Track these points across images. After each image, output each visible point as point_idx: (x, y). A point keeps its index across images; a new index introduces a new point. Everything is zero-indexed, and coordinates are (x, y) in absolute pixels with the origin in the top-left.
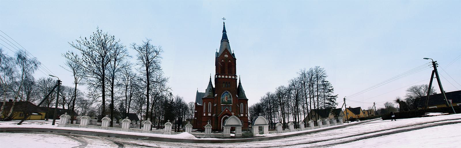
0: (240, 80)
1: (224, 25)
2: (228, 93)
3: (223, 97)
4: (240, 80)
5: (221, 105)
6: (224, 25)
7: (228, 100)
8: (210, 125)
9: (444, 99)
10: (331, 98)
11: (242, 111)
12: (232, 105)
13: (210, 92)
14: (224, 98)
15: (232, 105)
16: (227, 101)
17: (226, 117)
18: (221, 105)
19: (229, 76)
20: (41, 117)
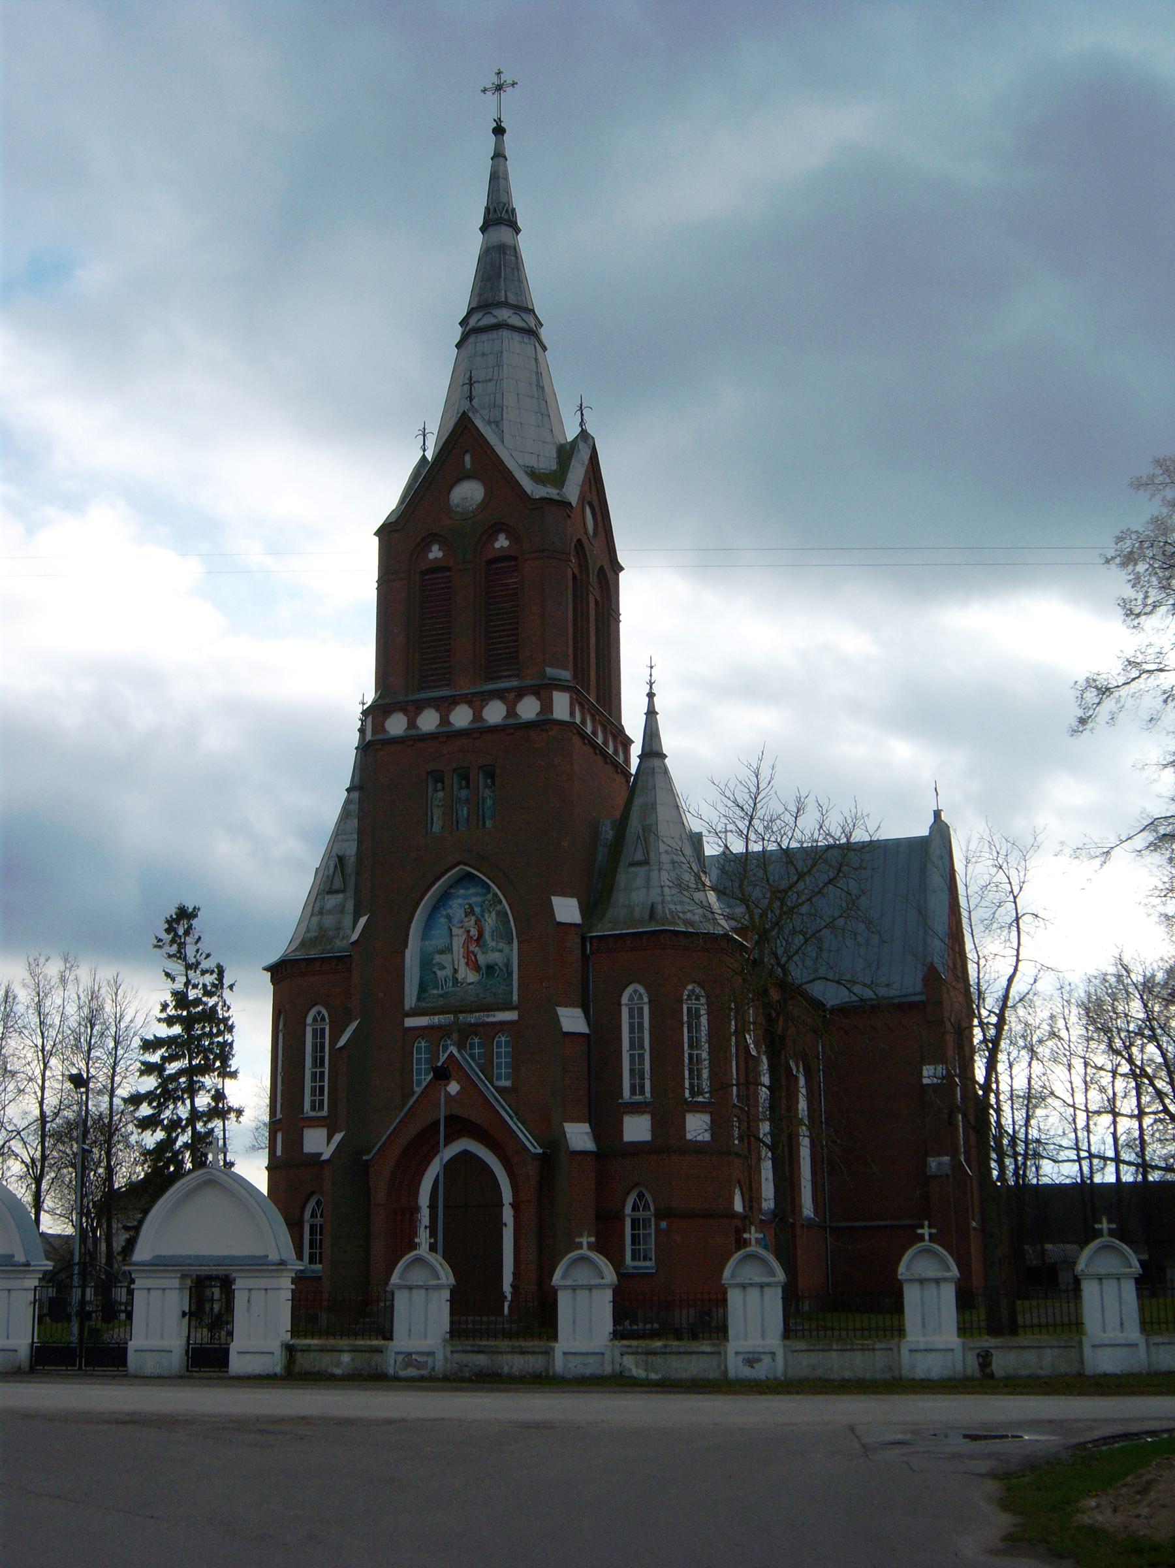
0: (651, 713)
1: (499, 155)
2: (488, 887)
3: (438, 939)
4: (651, 713)
5: (410, 1022)
6: (499, 155)
7: (482, 959)
8: (764, 1261)
9: (203, 1062)
10: (87, 1034)
11: (636, 1073)
12: (510, 1016)
13: (331, 892)
14: (449, 949)
15: (510, 1016)
16: (472, 977)
17: (466, 1153)
18: (410, 1022)
19: (449, 710)
20: (1123, 1115)
